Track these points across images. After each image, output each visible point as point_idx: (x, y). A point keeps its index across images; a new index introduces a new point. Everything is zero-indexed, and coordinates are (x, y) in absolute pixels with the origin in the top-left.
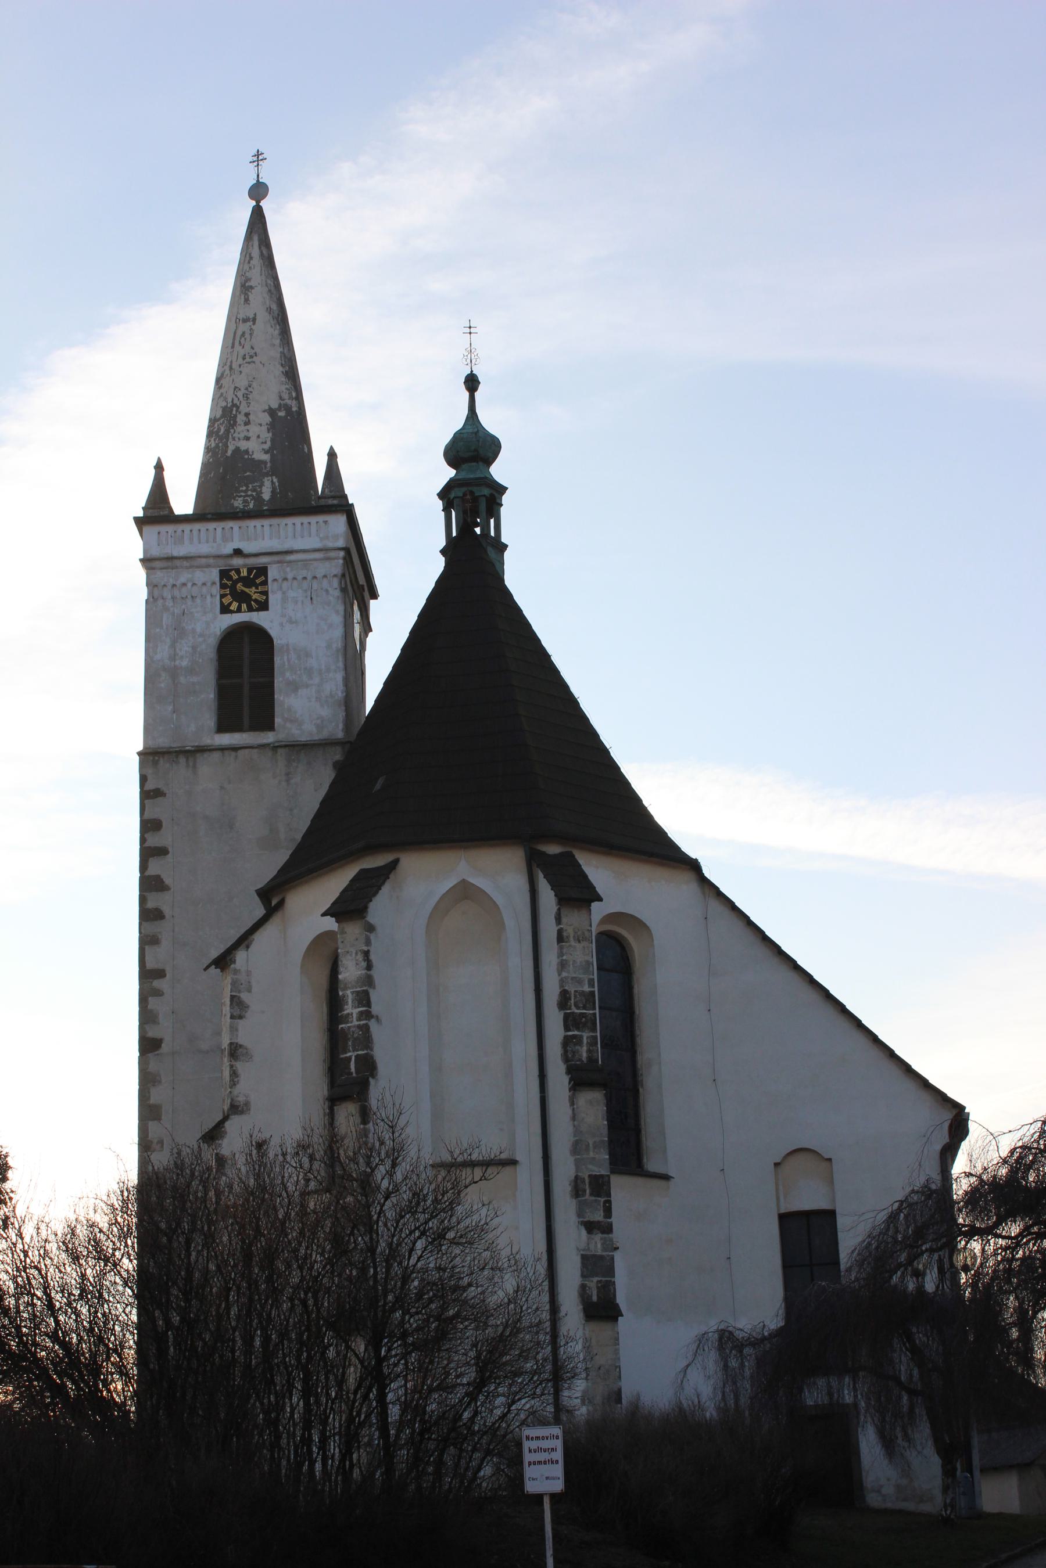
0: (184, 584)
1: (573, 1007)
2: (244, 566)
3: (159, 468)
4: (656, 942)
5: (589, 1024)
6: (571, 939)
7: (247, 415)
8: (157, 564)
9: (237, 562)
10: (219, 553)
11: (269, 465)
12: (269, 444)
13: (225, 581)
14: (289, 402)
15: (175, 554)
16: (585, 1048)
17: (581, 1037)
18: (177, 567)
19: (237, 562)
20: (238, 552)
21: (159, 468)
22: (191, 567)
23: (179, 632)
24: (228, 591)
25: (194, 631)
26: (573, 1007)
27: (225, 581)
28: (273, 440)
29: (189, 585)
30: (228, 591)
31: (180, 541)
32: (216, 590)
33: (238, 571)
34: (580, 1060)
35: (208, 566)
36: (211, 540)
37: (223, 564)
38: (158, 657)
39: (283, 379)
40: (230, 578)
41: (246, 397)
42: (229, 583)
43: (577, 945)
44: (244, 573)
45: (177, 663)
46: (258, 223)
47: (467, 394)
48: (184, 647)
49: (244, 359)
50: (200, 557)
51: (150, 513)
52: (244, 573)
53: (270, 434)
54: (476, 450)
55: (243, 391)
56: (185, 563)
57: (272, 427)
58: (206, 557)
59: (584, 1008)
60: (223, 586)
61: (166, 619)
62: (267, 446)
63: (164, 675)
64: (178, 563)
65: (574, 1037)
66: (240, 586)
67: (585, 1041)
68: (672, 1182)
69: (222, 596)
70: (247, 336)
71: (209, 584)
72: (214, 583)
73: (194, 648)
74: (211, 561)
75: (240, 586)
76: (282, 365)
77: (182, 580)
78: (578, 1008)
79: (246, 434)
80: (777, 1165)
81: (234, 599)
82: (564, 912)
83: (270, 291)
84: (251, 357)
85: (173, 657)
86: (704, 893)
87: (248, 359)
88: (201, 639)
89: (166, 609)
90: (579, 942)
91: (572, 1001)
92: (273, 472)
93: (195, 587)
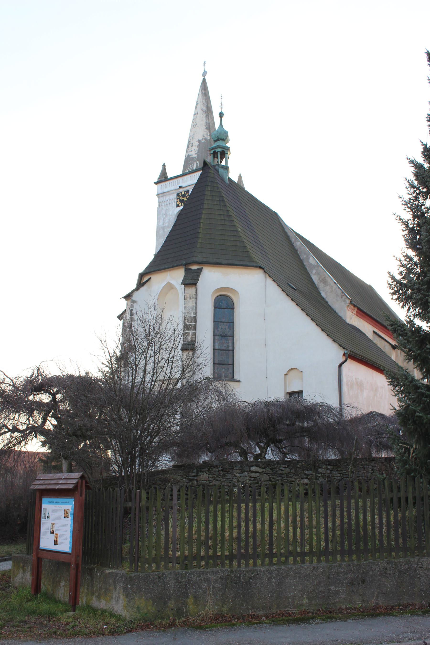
0: (167, 200)
1: (187, 322)
2: (183, 191)
3: (164, 166)
4: (240, 297)
5: (192, 328)
6: (188, 298)
7: (192, 144)
8: (160, 195)
9: (181, 190)
10: (176, 188)
11: (196, 158)
12: (197, 151)
13: (178, 197)
14: (206, 137)
15: (165, 191)
16: (190, 337)
17: (189, 333)
18: (165, 195)
19: (181, 190)
20: (180, 187)
21: (164, 166)
22: (169, 194)
23: (166, 215)
24: (178, 200)
25: (169, 214)
26: (187, 322)
27: (178, 197)
28: (198, 150)
29: (169, 200)
30: (178, 200)
31: (166, 187)
32: (176, 200)
33: (181, 193)
34: (188, 341)
35: (174, 193)
36: (174, 185)
37: (177, 192)
38: (160, 224)
39: (205, 130)
40: (179, 196)
41: (193, 138)
42: (179, 197)
43: (190, 300)
44: (183, 193)
45: (165, 225)
46: (204, 81)
47: (220, 119)
48: (167, 220)
49: (193, 126)
50: (171, 191)
51: (159, 180)
52: (183, 193)
53: (198, 148)
54: (218, 137)
55: (192, 136)
56: (167, 194)
57: (199, 146)
58: (172, 190)
59: (191, 322)
60: (177, 199)
61: (162, 212)
62: (196, 152)
63: (161, 229)
64: (165, 194)
65: (186, 333)
66: (181, 198)
67: (190, 334)
68: (241, 383)
69: (177, 202)
70: (195, 119)
71: (174, 199)
72: (175, 198)
73: (169, 220)
74: (174, 191)
75: (181, 198)
76: (205, 126)
77: (167, 199)
78: (189, 323)
79: (191, 150)
80: (286, 374)
81: (180, 202)
82: (186, 289)
83: (204, 104)
84: (195, 125)
85: (163, 224)
86: (266, 277)
87: (194, 126)
88: (171, 217)
89: (162, 209)
90: (191, 299)
91: (187, 320)
92: (197, 160)
93: (170, 201)
